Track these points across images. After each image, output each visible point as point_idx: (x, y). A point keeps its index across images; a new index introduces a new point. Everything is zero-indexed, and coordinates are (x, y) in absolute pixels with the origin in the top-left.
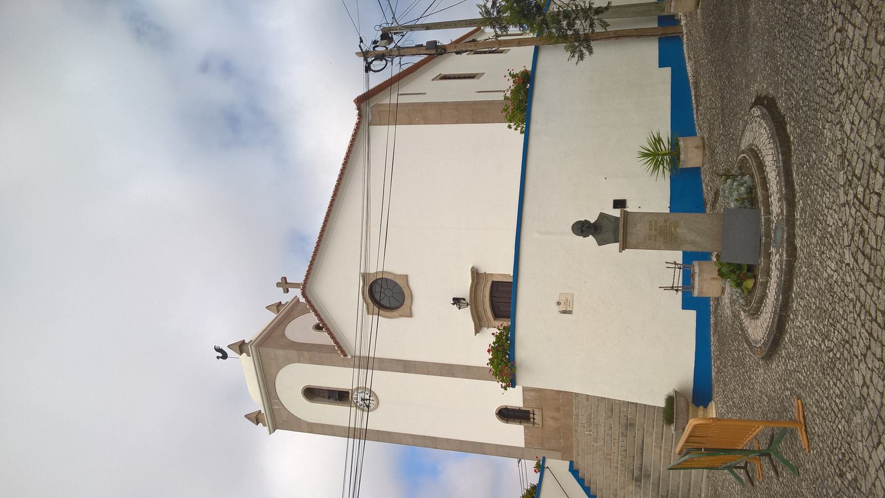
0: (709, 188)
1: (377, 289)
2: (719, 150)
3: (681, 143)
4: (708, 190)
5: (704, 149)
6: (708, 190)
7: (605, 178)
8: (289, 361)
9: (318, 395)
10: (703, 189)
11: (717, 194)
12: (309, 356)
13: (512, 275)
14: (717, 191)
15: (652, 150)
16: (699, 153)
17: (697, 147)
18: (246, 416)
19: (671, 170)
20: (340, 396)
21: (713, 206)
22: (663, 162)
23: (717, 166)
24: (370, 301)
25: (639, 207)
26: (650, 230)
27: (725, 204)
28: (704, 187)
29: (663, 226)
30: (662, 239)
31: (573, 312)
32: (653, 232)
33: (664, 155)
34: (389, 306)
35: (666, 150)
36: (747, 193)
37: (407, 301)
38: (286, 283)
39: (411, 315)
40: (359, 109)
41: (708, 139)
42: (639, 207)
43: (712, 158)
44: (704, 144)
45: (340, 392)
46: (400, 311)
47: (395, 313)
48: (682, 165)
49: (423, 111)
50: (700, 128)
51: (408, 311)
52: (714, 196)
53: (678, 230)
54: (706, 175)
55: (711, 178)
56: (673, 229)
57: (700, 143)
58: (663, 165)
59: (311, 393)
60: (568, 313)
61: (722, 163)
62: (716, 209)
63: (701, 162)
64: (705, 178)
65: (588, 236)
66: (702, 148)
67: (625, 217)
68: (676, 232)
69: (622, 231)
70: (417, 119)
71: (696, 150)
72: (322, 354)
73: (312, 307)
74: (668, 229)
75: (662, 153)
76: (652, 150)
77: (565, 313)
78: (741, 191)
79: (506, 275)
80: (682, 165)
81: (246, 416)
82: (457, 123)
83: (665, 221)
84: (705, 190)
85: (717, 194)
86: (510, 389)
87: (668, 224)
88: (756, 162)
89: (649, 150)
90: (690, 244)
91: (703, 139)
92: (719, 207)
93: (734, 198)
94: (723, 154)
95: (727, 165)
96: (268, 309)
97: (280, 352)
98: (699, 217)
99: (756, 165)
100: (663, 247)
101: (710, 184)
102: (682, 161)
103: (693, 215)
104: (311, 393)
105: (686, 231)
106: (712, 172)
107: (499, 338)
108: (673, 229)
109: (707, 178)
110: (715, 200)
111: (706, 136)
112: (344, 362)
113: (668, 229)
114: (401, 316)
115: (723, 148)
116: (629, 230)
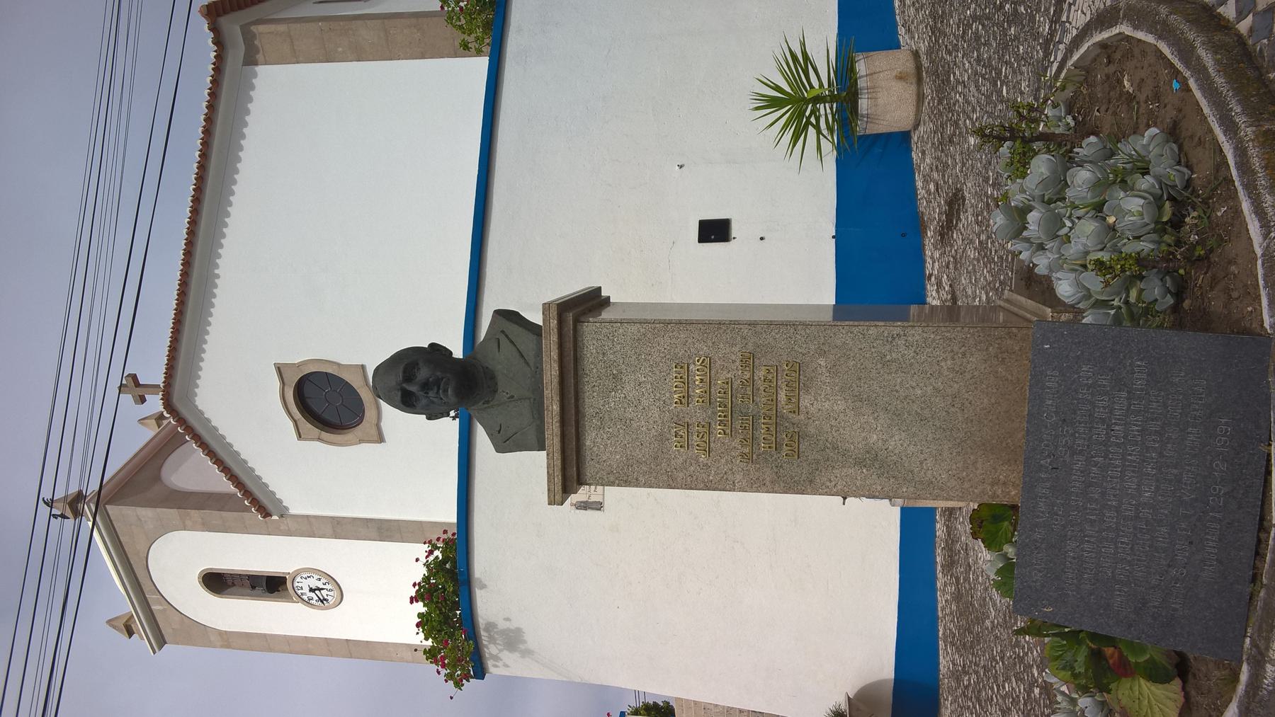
0: (932, 187)
1: (308, 390)
2: (964, 69)
3: (861, 67)
4: (929, 192)
5: (919, 81)
6: (929, 192)
7: (681, 167)
8: (165, 529)
9: (234, 585)
10: (915, 189)
11: (955, 203)
12: (202, 519)
14: (955, 195)
15: (788, 89)
16: (909, 91)
17: (901, 78)
18: (110, 622)
19: (839, 148)
20: (273, 586)
21: (942, 235)
22: (818, 119)
23: (956, 124)
24: (298, 415)
25: (762, 239)
26: (686, 399)
27: (983, 237)
28: (919, 184)
29: (737, 383)
30: (736, 444)
31: (606, 505)
32: (696, 412)
33: (817, 99)
34: (338, 422)
35: (821, 85)
36: (1160, 228)
38: (137, 384)
39: (381, 439)
40: (214, 28)
41: (930, 52)
42: (762, 239)
43: (940, 102)
44: (919, 68)
45: (268, 578)
46: (358, 431)
47: (350, 436)
48: (862, 128)
49: (351, 32)
50: (909, 31)
51: (374, 432)
52: (945, 208)
53: (806, 401)
54: (923, 153)
55: (938, 159)
56: (782, 396)
57: (910, 66)
58: (817, 127)
59: (216, 582)
60: (593, 509)
61: (974, 110)
62: (952, 246)
63: (912, 117)
64: (922, 158)
65: (433, 414)
66: (914, 80)
67: (569, 345)
68: (797, 410)
69: (556, 407)
70: (340, 49)
71: (898, 87)
72: (224, 514)
73: (190, 429)
74: (762, 399)
75: (813, 94)
76: (788, 89)
77: (585, 508)
78: (1120, 213)
80: (862, 128)
81: (110, 622)
82: (423, 57)
83: (749, 360)
84: (921, 192)
85: (955, 203)
86: (472, 685)
87: (761, 373)
88: (1215, 48)
89: (777, 88)
90: (860, 463)
91: (916, 55)
92: (960, 242)
93: (1073, 250)
94: (976, 82)
95: (990, 115)
96: (142, 424)
97: (146, 513)
98: (901, 342)
99: (1218, 62)
100: (739, 477)
101: (935, 175)
102: (863, 116)
103: (872, 331)
104: (216, 582)
105: (841, 405)
106: (941, 143)
107: (435, 569)
108: (782, 396)
109: (928, 161)
110: (949, 220)
111: (923, 47)
112: (268, 528)
113: (762, 399)
114: (361, 441)
115: (979, 60)
116: (592, 401)
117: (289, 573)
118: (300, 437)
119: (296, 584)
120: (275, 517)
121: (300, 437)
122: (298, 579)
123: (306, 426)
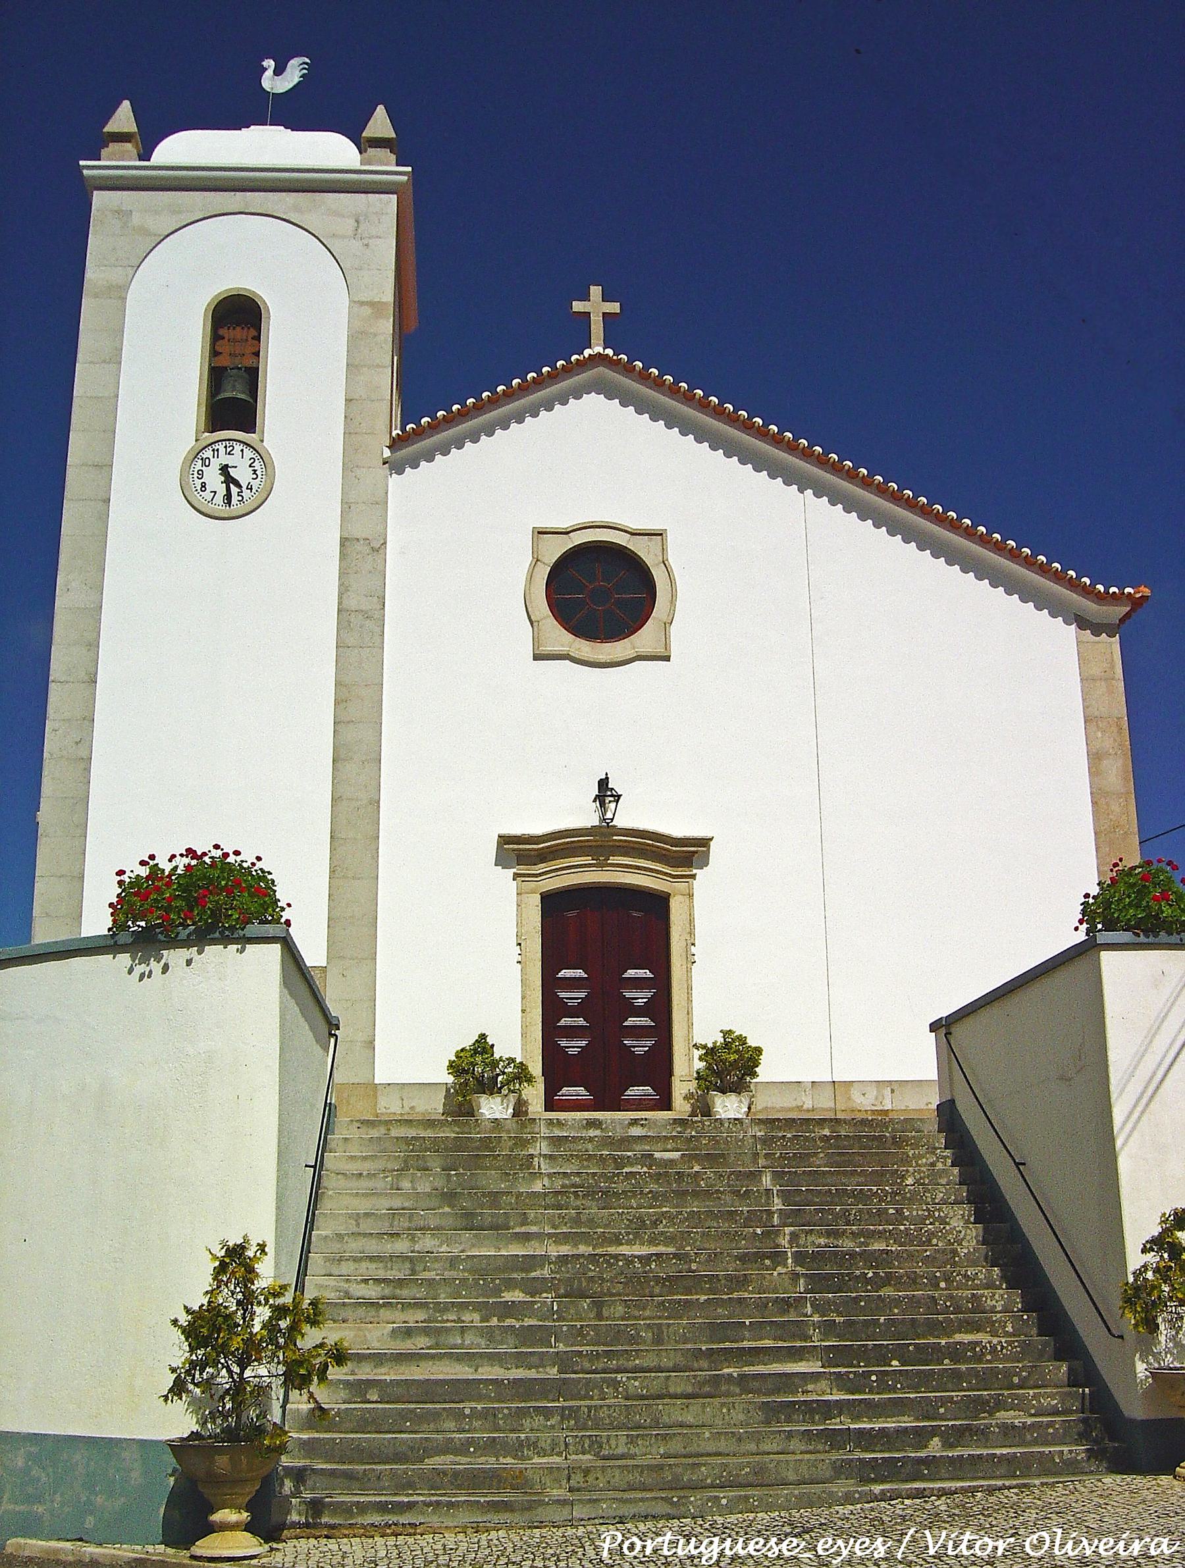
13: (85, 933)
37: (584, 648)
79: (691, 933)
117: (262, 441)
118: (539, 533)
119: (238, 447)
120: (387, 453)
121: (539, 533)
122: (249, 453)
123: (644, 550)
